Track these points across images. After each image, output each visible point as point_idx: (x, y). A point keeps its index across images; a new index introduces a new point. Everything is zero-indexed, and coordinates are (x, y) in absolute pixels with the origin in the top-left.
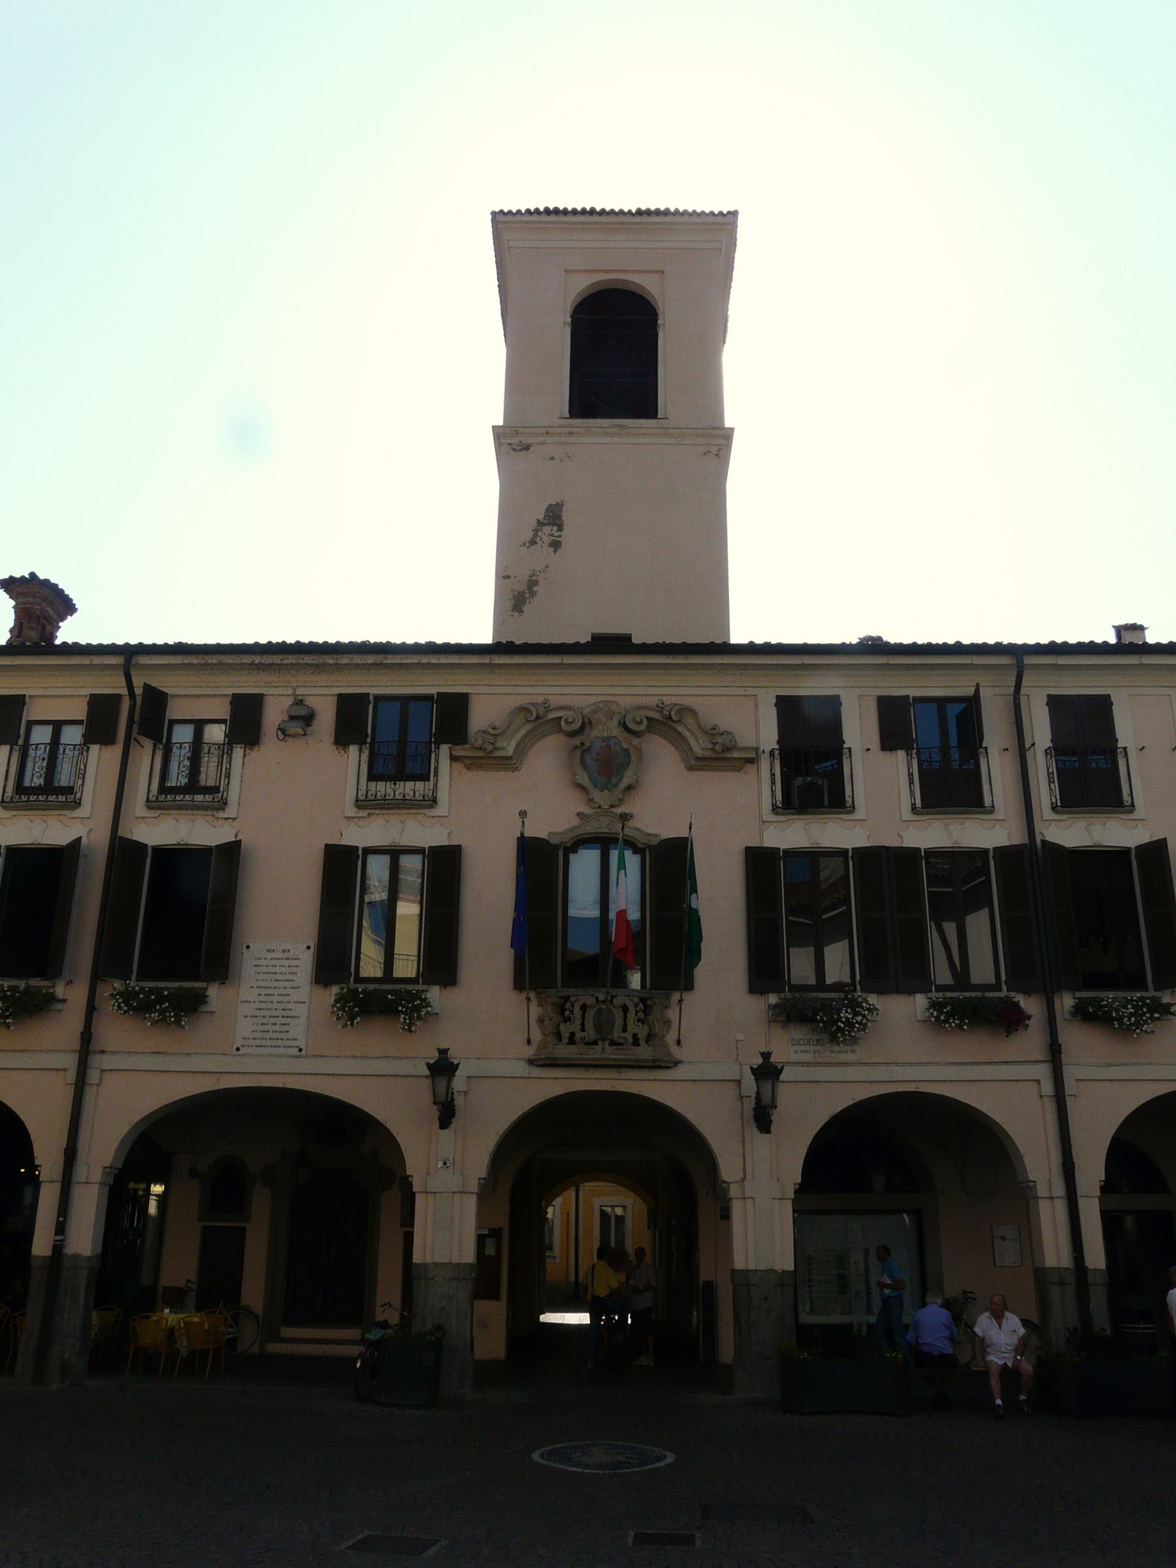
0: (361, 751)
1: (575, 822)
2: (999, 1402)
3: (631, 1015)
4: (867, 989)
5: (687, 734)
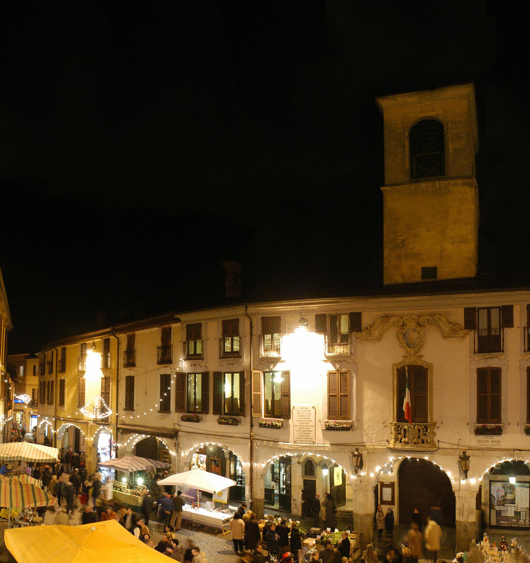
0: (474, 331)
1: (402, 359)
2: (290, 537)
3: (421, 432)
4: (18, 394)
5: (442, 325)
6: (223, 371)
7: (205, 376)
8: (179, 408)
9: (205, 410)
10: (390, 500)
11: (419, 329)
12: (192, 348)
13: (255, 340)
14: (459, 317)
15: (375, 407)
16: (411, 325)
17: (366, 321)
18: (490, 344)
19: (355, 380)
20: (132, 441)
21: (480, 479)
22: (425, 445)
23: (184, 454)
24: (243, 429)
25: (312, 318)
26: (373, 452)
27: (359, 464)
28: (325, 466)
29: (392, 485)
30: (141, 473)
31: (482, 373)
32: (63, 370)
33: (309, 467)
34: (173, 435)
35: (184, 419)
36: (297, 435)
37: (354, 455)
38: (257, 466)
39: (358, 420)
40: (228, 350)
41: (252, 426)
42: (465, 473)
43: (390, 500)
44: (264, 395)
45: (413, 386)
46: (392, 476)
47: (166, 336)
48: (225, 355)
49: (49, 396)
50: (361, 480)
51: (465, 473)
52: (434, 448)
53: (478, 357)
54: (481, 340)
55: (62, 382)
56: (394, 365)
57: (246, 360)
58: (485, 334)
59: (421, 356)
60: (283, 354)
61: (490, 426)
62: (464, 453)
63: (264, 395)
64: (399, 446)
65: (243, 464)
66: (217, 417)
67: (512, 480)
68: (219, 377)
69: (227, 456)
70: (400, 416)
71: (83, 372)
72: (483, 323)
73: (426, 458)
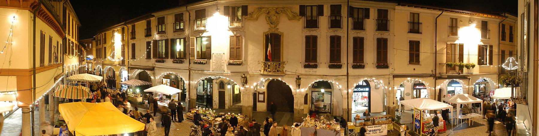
6: (175, 38)
7: (167, 41)
8: (155, 56)
9: (167, 57)
10: (262, 100)
11: (277, 14)
12: (160, 28)
13: (191, 23)
14: (297, 9)
15: (254, 54)
16: (273, 13)
17: (250, 10)
18: (312, 24)
19: (244, 40)
20: (135, 73)
21: (306, 89)
22: (279, 72)
23: (157, 78)
24: (186, 65)
25: (222, 9)
26: (253, 76)
27: (245, 82)
28: (229, 84)
29: (264, 93)
30: (137, 87)
31: (308, 38)
32: (105, 43)
33: (222, 85)
34: (152, 69)
35: (156, 61)
36: (214, 67)
37: (242, 77)
38: (195, 83)
39: (245, 60)
40: (178, 28)
41: (190, 63)
42: (299, 86)
43: (262, 100)
44: (197, 49)
45: (273, 44)
46: (264, 89)
47: (149, 24)
48: (176, 31)
49: (101, 54)
50: (246, 89)
51: (299, 86)
52: (283, 74)
53: (306, 30)
54: (307, 21)
55: (105, 48)
56: (264, 33)
57: (187, 32)
58: (310, 19)
59: (278, 29)
60: (207, 28)
61: (312, 64)
62: (298, 76)
63: (197, 49)
64: (266, 73)
65: (185, 82)
66: (172, 60)
67: (323, 90)
68: (173, 41)
69: (180, 79)
70: (267, 59)
71: (114, 43)
72: (309, 13)
73: (280, 79)
